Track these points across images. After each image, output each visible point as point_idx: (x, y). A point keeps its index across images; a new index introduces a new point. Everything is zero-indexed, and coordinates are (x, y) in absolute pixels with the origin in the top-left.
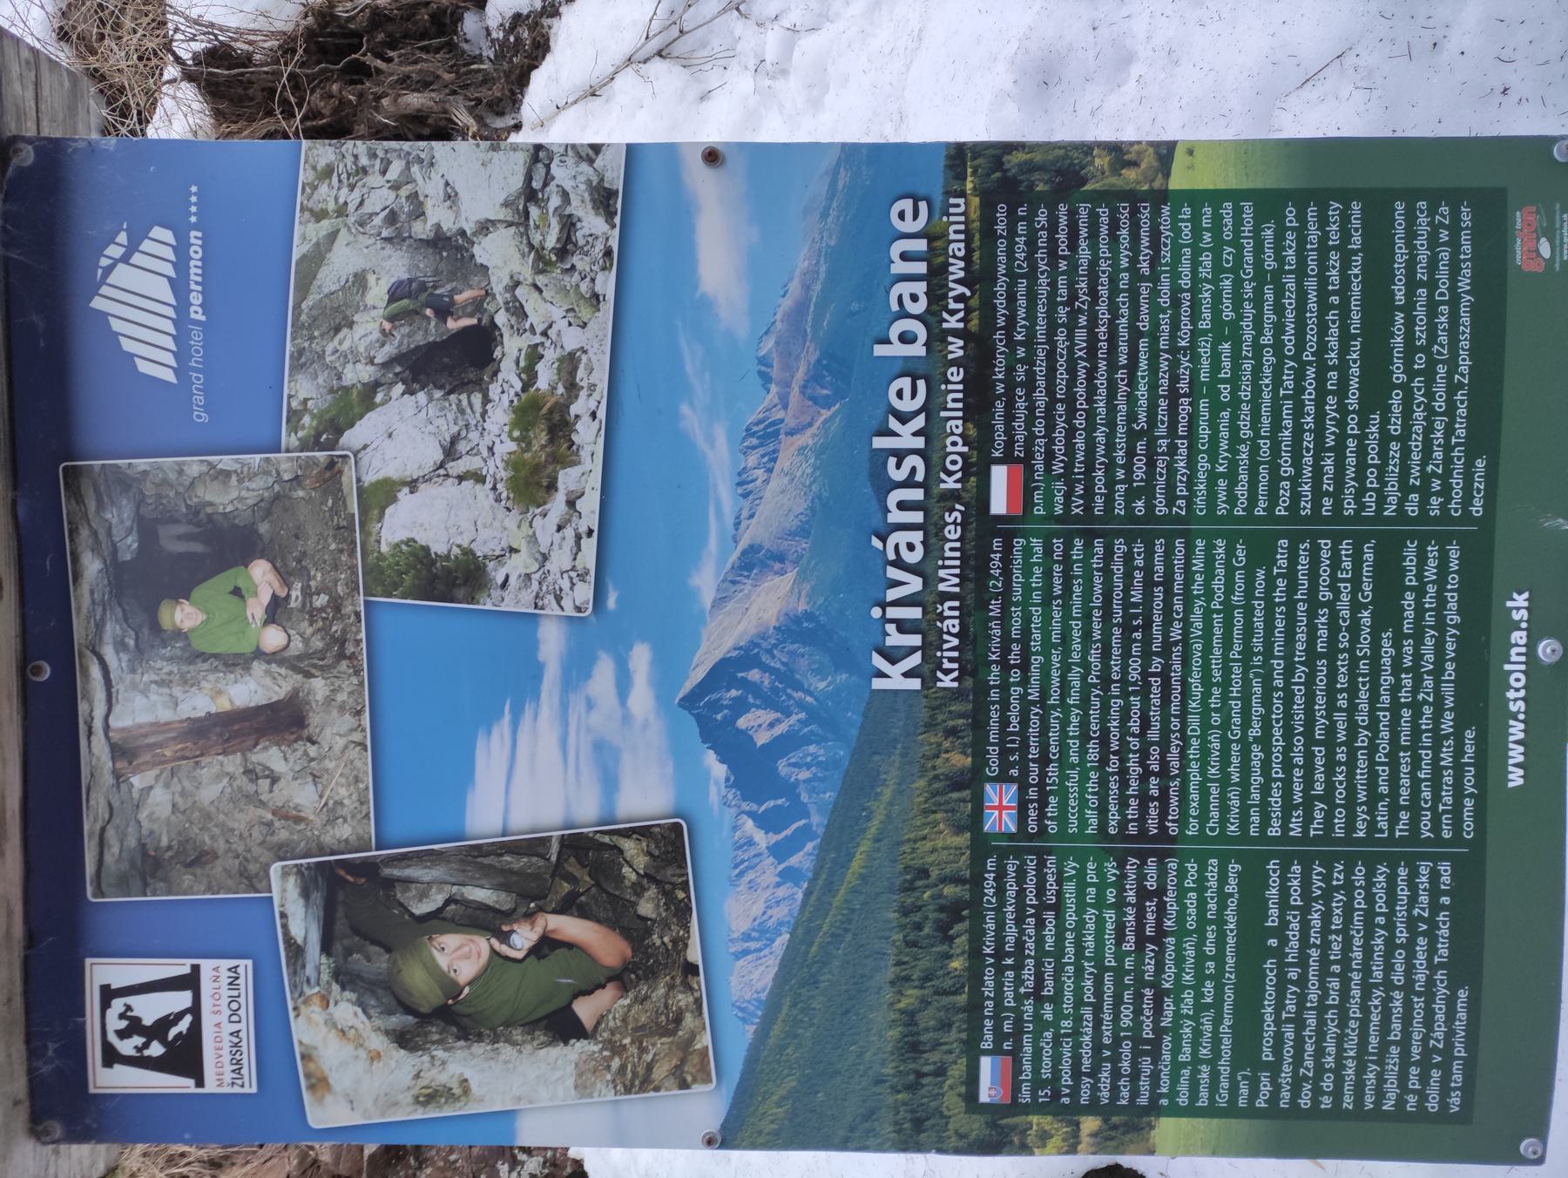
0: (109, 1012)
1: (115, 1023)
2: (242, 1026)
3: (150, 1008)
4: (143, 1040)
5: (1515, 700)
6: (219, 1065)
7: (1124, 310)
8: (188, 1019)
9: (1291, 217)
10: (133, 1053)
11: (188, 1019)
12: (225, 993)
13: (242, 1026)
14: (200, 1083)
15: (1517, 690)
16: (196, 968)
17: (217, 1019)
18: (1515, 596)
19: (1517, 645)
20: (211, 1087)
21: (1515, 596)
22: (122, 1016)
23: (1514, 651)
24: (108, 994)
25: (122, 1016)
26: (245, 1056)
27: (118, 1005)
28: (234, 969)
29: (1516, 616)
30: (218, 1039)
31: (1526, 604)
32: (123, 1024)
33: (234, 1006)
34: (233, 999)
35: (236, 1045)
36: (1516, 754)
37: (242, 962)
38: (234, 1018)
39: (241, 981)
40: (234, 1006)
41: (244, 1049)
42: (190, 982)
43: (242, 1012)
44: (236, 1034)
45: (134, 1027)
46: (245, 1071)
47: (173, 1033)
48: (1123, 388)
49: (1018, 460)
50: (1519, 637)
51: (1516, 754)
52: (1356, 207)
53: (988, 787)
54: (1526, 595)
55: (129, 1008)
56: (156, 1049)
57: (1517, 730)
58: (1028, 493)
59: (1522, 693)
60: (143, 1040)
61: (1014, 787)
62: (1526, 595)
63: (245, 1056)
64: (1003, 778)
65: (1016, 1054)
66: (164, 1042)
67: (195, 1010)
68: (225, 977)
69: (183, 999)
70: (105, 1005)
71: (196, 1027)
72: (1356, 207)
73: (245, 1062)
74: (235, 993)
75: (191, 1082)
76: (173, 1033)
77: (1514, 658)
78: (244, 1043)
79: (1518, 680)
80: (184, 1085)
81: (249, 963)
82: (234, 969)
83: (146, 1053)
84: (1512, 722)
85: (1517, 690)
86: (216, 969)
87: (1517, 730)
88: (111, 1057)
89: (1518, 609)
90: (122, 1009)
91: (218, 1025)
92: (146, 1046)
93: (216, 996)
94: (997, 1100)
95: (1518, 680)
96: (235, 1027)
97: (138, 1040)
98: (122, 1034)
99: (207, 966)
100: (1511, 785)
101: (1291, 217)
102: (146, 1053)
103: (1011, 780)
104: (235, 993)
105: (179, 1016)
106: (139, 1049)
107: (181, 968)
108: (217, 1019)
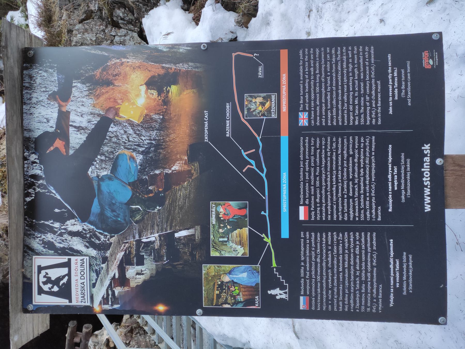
0: (40, 275)
1: (42, 279)
2: (85, 280)
3: (54, 274)
4: (52, 285)
5: (426, 181)
6: (77, 295)
7: (329, 176)
8: (67, 278)
9: (362, 140)
10: (48, 290)
11: (67, 278)
12: (79, 268)
13: (85, 280)
14: (70, 301)
15: (427, 178)
16: (70, 260)
17: (76, 278)
18: (425, 145)
19: (426, 162)
20: (74, 303)
21: (425, 145)
22: (45, 277)
23: (425, 164)
24: (40, 269)
25: (45, 277)
26: (86, 291)
27: (43, 272)
28: (82, 260)
29: (425, 152)
30: (77, 285)
31: (429, 148)
32: (45, 279)
33: (82, 273)
34: (82, 271)
35: (83, 287)
36: (427, 200)
37: (85, 258)
38: (82, 278)
39: (85, 264)
40: (82, 273)
41: (86, 289)
42: (67, 265)
43: (85, 276)
44: (83, 283)
45: (48, 280)
46: (86, 297)
47: (61, 283)
48: (329, 197)
49: (307, 205)
50: (427, 159)
51: (427, 200)
52: (373, 137)
53: (300, 113)
54: (429, 145)
55: (47, 274)
56: (56, 289)
57: (427, 191)
58: (310, 212)
59: (429, 179)
60: (52, 285)
61: (307, 113)
62: (429, 145)
63: (86, 291)
64: (304, 110)
65: (310, 206)
66: (58, 286)
67: (69, 275)
68: (79, 262)
69: (65, 271)
70: (39, 272)
71: (69, 281)
72: (373, 137)
73: (86, 294)
74: (83, 269)
75: (67, 301)
76: (61, 283)
77: (425, 167)
78: (86, 287)
79: (427, 174)
80: (63, 302)
81: (88, 258)
82: (82, 260)
83: (52, 290)
84: (425, 189)
85: (427, 178)
86: (76, 260)
87: (427, 191)
88: (41, 291)
89: (426, 150)
90: (45, 274)
91: (77, 280)
92: (52, 287)
93: (76, 269)
94: (305, 309)
95: (427, 174)
96: (83, 281)
97: (50, 285)
98: (45, 283)
99: (73, 259)
100: (426, 211)
101: (362, 140)
102: (52, 290)
103: (306, 111)
104: (83, 269)
105: (64, 277)
106: (50, 289)
107: (64, 259)
108: (76, 278)
